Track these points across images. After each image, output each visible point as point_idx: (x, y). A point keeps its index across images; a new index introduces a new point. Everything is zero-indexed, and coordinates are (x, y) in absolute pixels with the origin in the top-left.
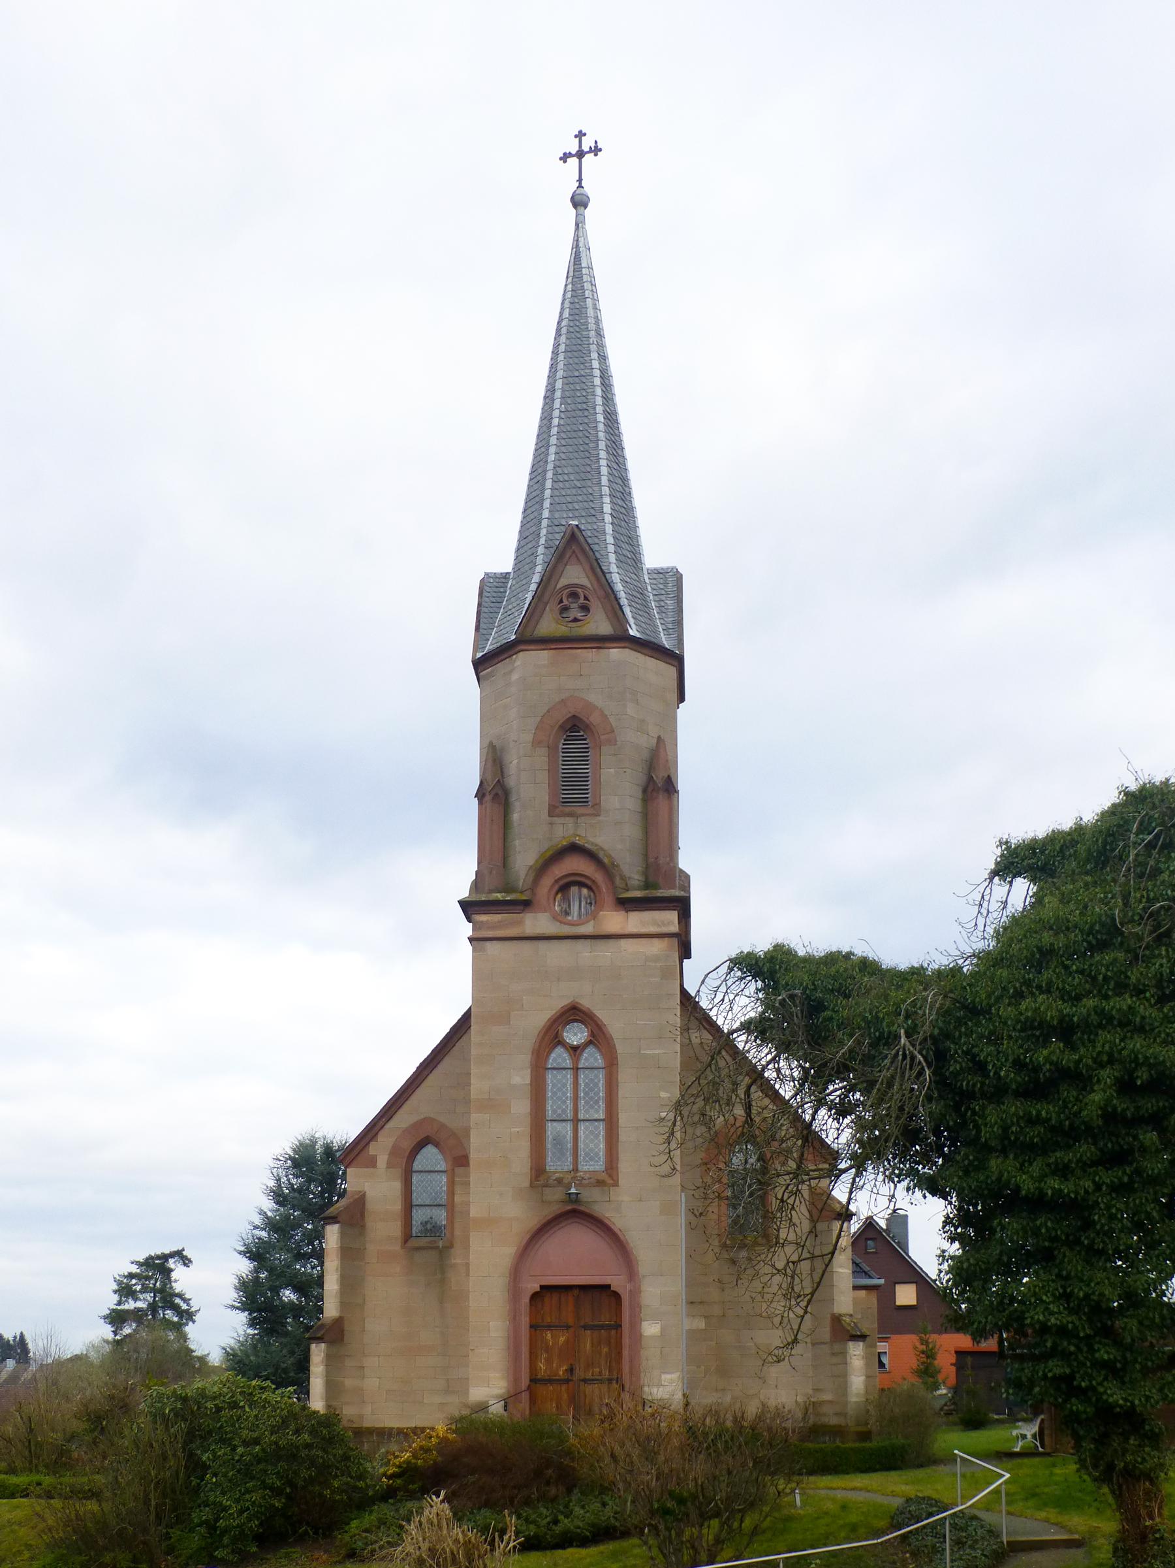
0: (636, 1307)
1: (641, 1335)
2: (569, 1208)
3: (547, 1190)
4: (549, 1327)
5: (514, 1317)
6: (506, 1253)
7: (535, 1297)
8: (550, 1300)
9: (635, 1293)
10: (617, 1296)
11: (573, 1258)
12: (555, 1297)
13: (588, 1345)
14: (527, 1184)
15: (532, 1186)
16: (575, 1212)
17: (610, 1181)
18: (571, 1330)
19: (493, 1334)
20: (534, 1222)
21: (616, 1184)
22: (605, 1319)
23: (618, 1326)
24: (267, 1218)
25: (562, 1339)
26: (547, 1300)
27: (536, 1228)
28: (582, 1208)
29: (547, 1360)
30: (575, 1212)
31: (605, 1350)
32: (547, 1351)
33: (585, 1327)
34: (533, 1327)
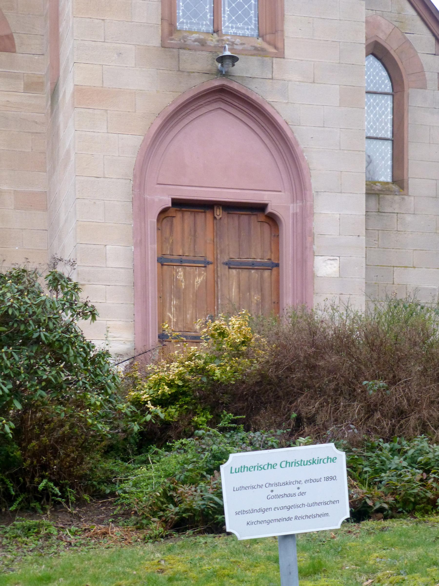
0: (305, 236)
1: (313, 275)
2: (217, 83)
3: (185, 54)
4: (181, 262)
5: (140, 244)
6: (129, 143)
7: (164, 213)
8: (184, 222)
9: (304, 217)
10: (273, 220)
11: (220, 160)
12: (188, 217)
13: (234, 291)
14: (156, 42)
15: (163, 46)
16: (224, 93)
17: (272, 50)
18: (210, 267)
19: (110, 264)
20: (168, 100)
21: (281, 55)
22: (258, 252)
23: (274, 266)
24: (230, 75)
25: (199, 280)
26: (177, 221)
27: (171, 109)
28: (235, 86)
29: (179, 308)
30: (224, 93)
31: (256, 298)
32: (178, 298)
33: (230, 265)
34: (162, 261)
